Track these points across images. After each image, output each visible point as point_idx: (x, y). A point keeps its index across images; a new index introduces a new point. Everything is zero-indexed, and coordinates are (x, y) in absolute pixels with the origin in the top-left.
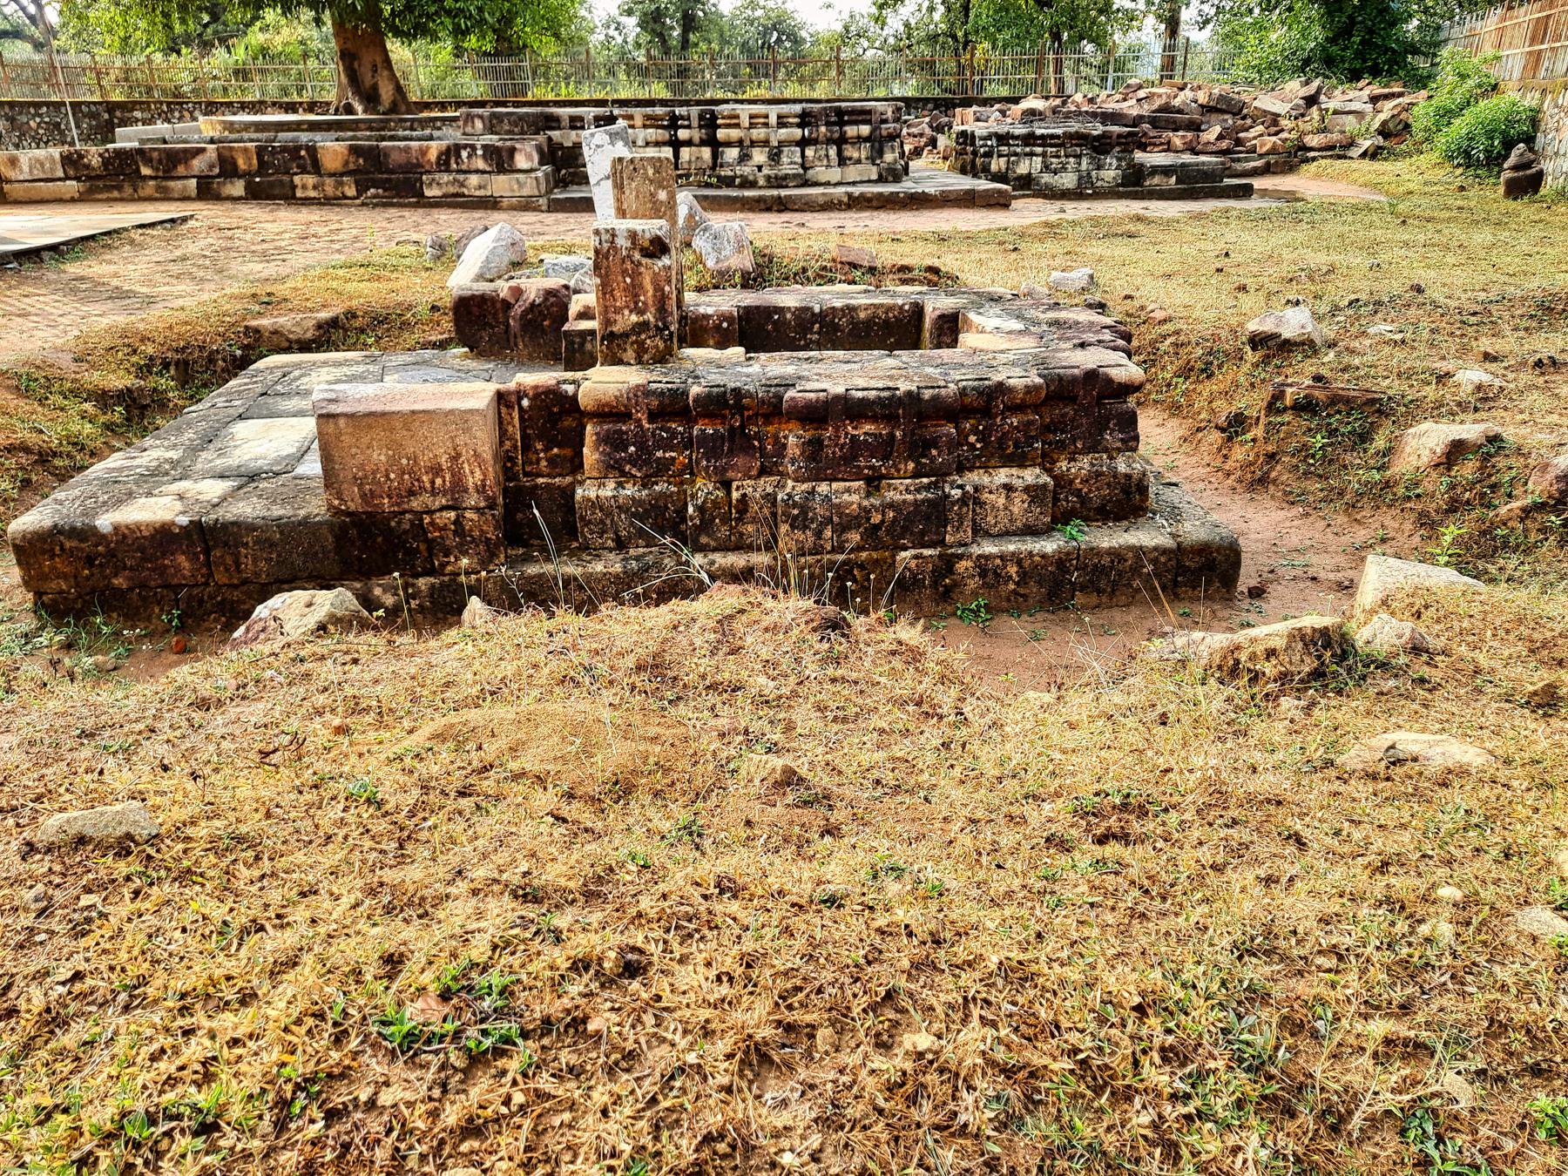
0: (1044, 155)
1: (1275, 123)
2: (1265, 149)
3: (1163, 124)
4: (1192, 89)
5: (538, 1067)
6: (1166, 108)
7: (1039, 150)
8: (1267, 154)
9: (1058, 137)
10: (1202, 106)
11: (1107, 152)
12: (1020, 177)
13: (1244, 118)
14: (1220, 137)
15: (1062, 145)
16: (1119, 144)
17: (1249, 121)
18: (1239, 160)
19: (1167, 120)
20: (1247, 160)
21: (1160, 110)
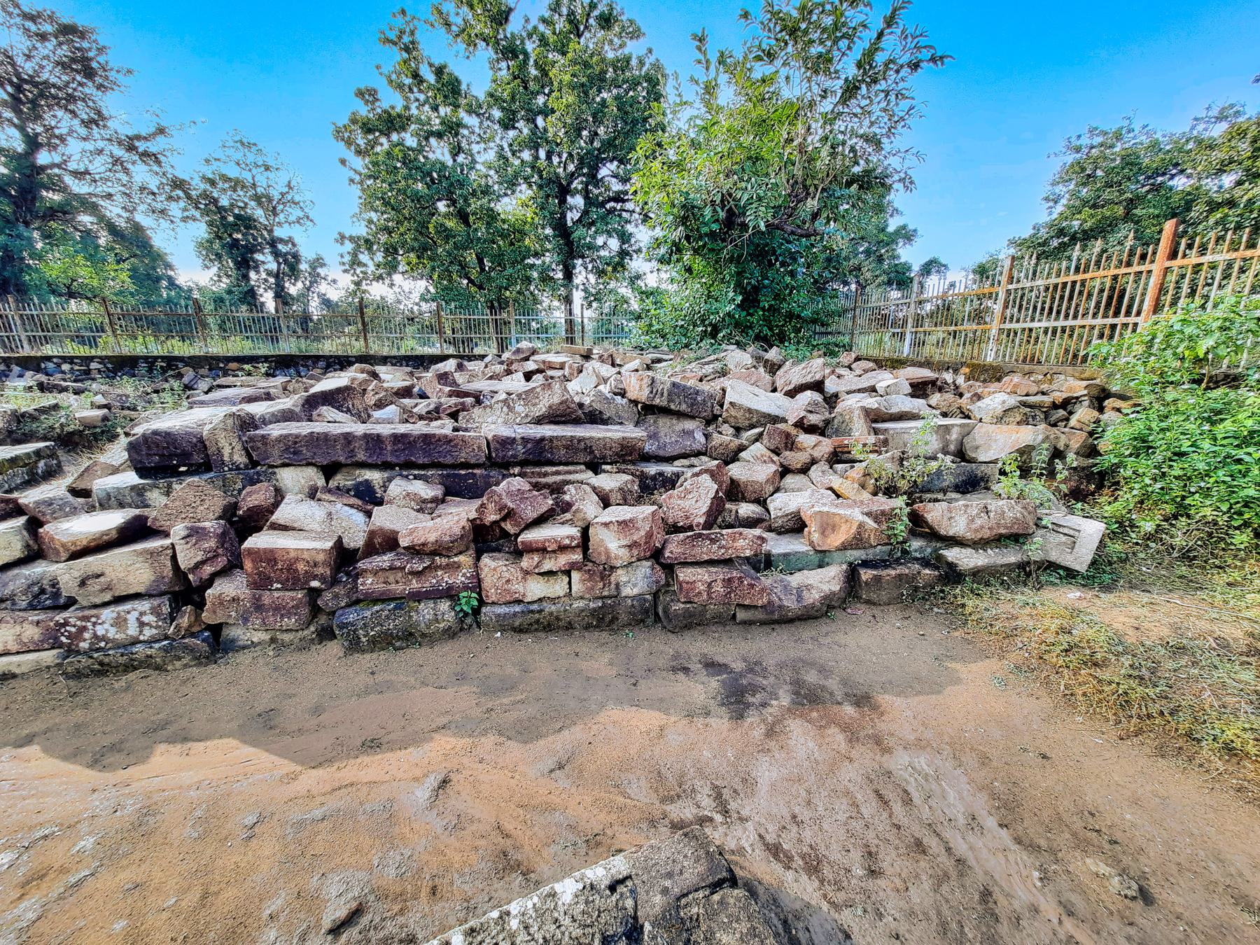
19: (572, 445)
21: (554, 417)
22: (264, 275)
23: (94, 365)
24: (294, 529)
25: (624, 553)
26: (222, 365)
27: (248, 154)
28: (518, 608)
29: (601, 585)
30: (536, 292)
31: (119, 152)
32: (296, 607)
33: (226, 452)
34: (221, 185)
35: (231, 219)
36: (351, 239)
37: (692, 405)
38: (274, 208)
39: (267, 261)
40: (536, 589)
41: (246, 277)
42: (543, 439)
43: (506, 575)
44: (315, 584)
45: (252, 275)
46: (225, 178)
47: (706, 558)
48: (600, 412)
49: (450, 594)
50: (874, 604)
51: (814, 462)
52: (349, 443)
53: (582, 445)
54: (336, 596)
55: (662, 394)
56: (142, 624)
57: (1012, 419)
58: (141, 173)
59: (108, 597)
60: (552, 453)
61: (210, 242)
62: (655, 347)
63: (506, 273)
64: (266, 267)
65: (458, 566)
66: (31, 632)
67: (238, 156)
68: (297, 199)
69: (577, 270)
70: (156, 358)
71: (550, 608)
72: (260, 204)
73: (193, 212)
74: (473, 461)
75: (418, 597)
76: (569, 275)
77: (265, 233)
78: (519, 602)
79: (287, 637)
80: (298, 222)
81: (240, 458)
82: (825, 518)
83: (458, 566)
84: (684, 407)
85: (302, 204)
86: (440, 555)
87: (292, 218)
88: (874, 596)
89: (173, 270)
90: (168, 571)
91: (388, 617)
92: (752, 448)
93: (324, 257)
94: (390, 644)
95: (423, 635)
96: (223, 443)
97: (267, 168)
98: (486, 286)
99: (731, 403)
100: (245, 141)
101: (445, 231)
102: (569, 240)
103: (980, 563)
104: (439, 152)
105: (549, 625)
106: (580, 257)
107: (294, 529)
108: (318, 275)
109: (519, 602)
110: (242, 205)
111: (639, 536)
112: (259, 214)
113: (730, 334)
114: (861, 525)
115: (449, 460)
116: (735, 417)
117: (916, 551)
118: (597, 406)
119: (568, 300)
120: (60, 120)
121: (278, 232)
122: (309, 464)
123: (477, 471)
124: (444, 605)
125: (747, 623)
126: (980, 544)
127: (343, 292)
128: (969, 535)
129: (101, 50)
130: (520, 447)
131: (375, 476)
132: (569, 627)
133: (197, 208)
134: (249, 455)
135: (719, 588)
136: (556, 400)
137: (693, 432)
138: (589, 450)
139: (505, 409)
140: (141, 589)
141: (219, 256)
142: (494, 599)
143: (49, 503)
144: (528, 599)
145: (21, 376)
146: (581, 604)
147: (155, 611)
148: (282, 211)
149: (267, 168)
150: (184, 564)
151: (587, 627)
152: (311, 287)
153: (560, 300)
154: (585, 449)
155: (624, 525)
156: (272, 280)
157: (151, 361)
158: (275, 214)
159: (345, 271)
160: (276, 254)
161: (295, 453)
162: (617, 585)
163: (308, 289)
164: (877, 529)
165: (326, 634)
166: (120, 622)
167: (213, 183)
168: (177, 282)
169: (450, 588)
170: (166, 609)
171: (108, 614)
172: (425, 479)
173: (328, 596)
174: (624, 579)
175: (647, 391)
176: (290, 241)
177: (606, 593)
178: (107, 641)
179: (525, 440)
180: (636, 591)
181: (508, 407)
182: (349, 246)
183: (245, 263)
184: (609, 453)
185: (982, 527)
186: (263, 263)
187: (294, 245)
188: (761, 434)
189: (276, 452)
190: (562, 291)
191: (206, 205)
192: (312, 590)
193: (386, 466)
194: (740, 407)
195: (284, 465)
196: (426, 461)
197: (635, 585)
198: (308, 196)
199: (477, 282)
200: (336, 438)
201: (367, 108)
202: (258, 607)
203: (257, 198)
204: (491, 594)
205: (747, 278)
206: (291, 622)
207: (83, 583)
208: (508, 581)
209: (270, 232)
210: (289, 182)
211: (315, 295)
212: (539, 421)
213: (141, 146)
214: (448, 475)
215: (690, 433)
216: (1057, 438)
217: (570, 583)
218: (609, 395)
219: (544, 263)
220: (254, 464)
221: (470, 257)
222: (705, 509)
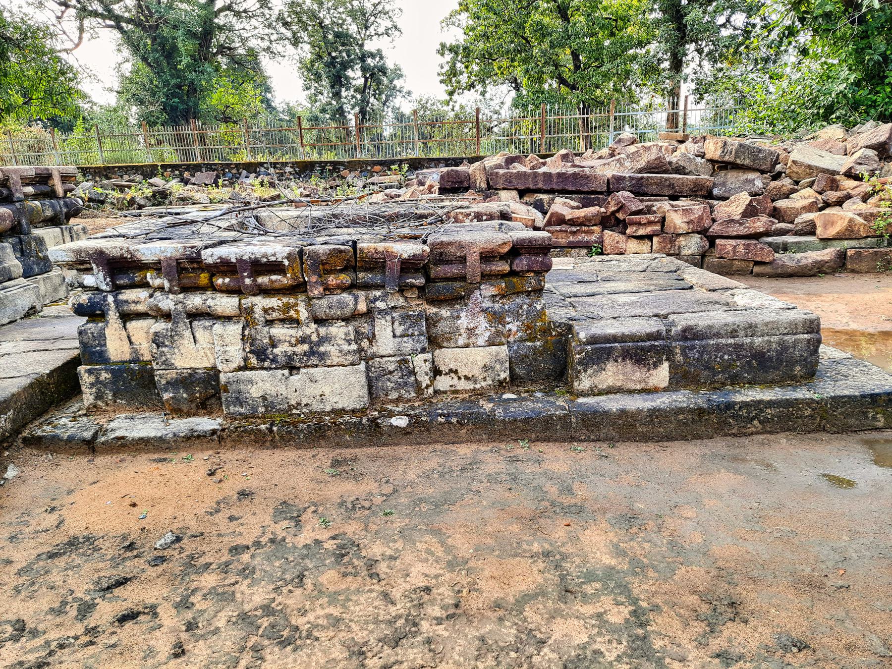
0: (245, 315)
1: (834, 185)
2: (832, 232)
3: (654, 189)
4: (695, 141)
5: (547, 554)
6: (657, 167)
7: (226, 304)
8: (839, 238)
9: (275, 267)
10: (712, 161)
11: (455, 299)
12: (187, 381)
13: (777, 177)
14: (750, 212)
15: (298, 288)
16: (487, 277)
17: (786, 183)
18: (785, 248)
19: (660, 183)
20: (800, 248)
21: (649, 169)
22: (352, 92)
23: (288, 169)
25: (684, 226)
26: (369, 168)
29: (669, 246)
30: (634, 87)
33: (478, 181)
37: (754, 160)
38: (367, 21)
39: (356, 76)
47: (735, 233)
48: (684, 168)
50: (858, 272)
51: (849, 197)
55: (731, 153)
60: (647, 188)
62: (762, 133)
63: (604, 69)
68: (387, 8)
69: (689, 57)
70: (326, 163)
72: (355, 19)
74: (599, 190)
76: (677, 65)
80: (387, 34)
81: (484, 185)
82: (827, 217)
83: (592, 232)
84: (747, 162)
85: (390, 13)
86: (585, 225)
87: (381, 30)
88: (856, 267)
89: (270, 92)
92: (802, 191)
93: (402, 67)
96: (478, 177)
98: (580, 85)
99: (793, 161)
101: (541, 29)
102: (681, 23)
106: (692, 41)
108: (395, 87)
110: (340, 22)
112: (353, 29)
113: (846, 115)
114: (851, 221)
115: (585, 189)
116: (797, 173)
118: (681, 163)
119: (674, 93)
121: (370, 46)
123: (601, 196)
125: (760, 275)
127: (416, 104)
131: (545, 197)
134: (488, 183)
135: (741, 249)
136: (653, 157)
137: (754, 180)
138: (672, 186)
139: (618, 165)
141: (318, 77)
142: (609, 251)
145: (247, 177)
153: (663, 95)
155: (686, 211)
156: (359, 96)
157: (323, 164)
158: (367, 28)
159: (442, 82)
162: (679, 247)
164: (865, 225)
168: (273, 104)
169: (588, 242)
172: (572, 199)
174: (684, 243)
175: (719, 151)
176: (379, 54)
180: (690, 252)
181: (620, 163)
182: (448, 57)
183: (338, 81)
186: (354, 79)
187: (381, 58)
188: (813, 182)
190: (668, 84)
193: (551, 191)
194: (802, 164)
195: (504, 189)
196: (573, 189)
197: (690, 248)
198: (395, 5)
199: (570, 81)
205: (869, 54)
208: (618, 242)
209: (361, 46)
211: (390, 109)
214: (584, 198)
215: (752, 181)
217: (651, 246)
218: (692, 157)
219: (648, 52)
220: (489, 187)
221: (565, 56)
222: (741, 211)
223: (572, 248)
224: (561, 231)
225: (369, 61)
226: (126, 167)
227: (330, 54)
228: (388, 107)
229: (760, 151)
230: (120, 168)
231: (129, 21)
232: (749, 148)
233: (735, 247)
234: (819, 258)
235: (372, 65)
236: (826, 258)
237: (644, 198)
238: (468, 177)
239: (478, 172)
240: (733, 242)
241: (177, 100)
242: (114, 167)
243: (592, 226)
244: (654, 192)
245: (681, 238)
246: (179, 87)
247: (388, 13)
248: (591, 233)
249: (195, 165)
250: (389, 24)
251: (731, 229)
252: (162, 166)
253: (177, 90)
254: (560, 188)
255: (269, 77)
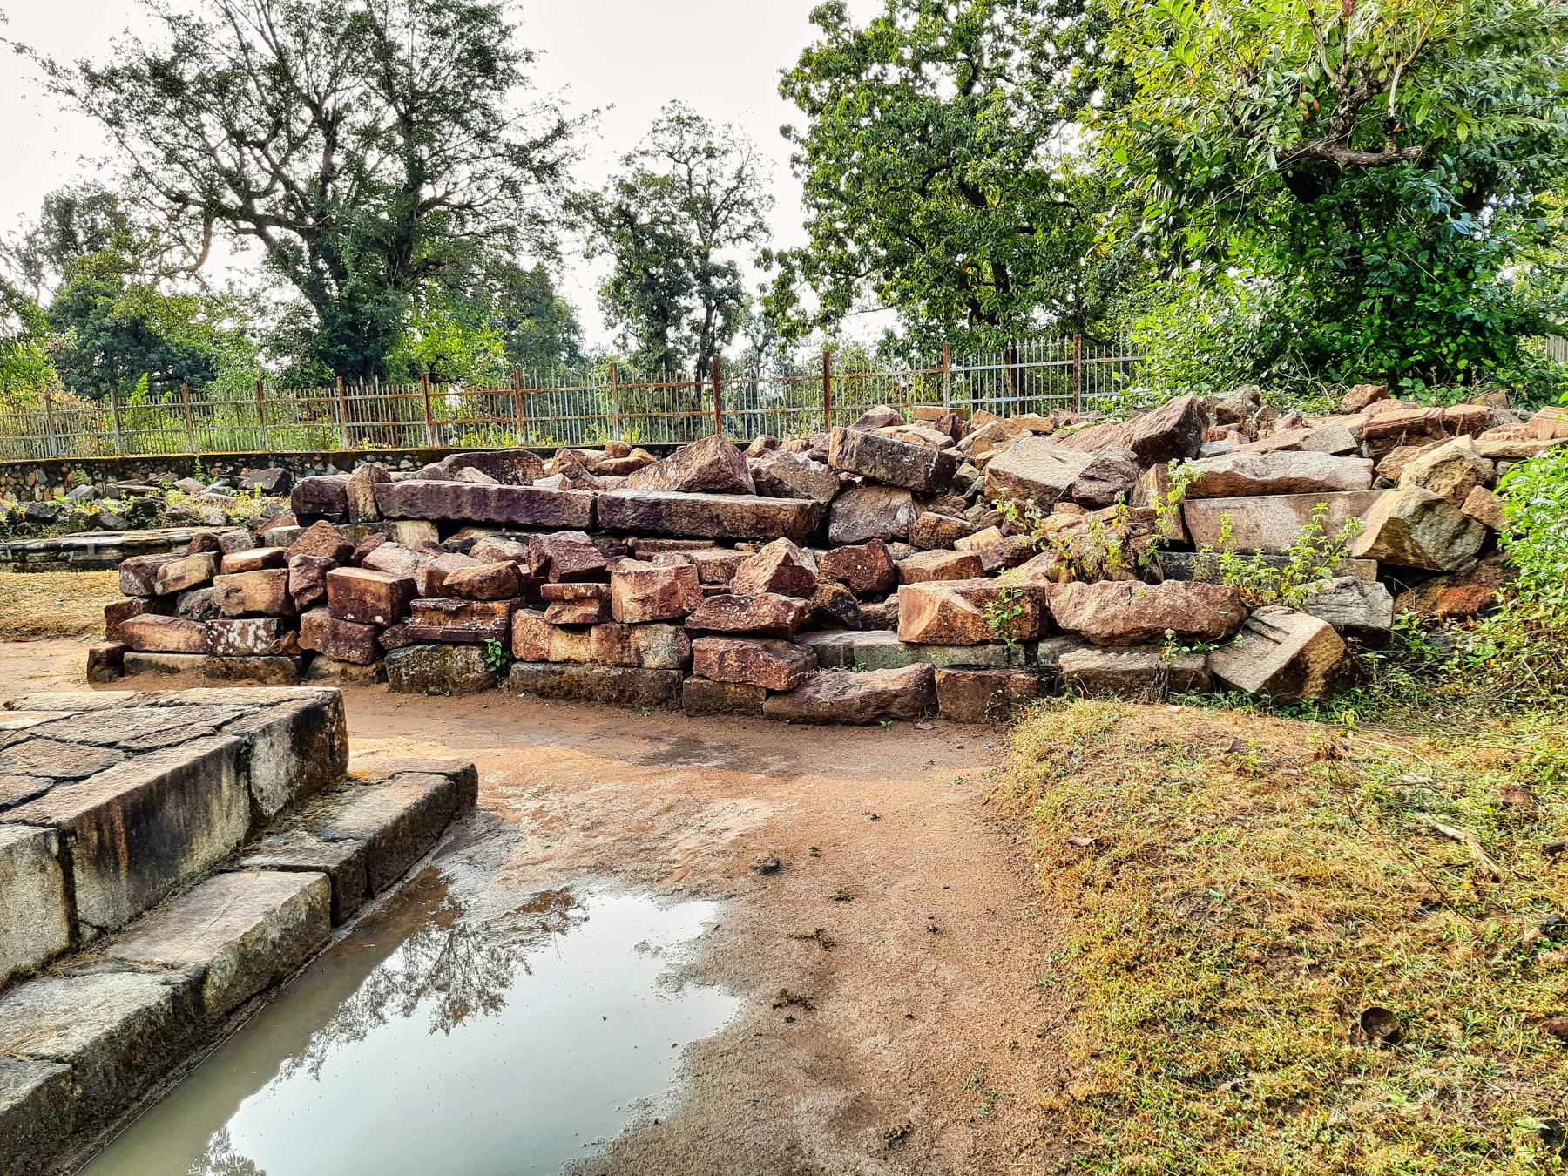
3: (683, 524)
22: (686, 331)
24: (379, 569)
27: (686, 136)
28: (541, 667)
31: (509, 170)
32: (361, 640)
33: (361, 502)
34: (642, 193)
35: (650, 245)
36: (782, 259)
37: (894, 470)
38: (715, 216)
39: (694, 306)
40: (561, 647)
41: (661, 336)
42: (657, 503)
43: (535, 628)
44: (379, 619)
45: (671, 333)
46: (649, 180)
47: (731, 626)
48: (781, 482)
49: (476, 640)
50: (957, 721)
52: (458, 497)
53: (706, 513)
54: (395, 634)
56: (257, 638)
57: (1445, 481)
58: (534, 195)
59: (240, 611)
61: (618, 285)
64: (692, 316)
65: (492, 614)
66: (196, 638)
67: (671, 141)
68: (749, 196)
71: (571, 670)
72: (694, 213)
73: (601, 240)
75: (456, 640)
77: (696, 261)
78: (545, 661)
79: (353, 671)
80: (746, 236)
83: (492, 614)
84: (881, 472)
85: (756, 204)
86: (477, 599)
87: (739, 230)
89: (576, 332)
90: (281, 595)
91: (426, 658)
94: (425, 687)
95: (455, 685)
96: (359, 494)
97: (711, 154)
99: (991, 471)
100: (684, 115)
103: (1091, 665)
104: (943, 84)
105: (570, 692)
107: (379, 569)
109: (545, 661)
111: (653, 589)
112: (692, 231)
114: (945, 607)
117: (1046, 657)
120: (456, 139)
122: (423, 519)
124: (475, 654)
126: (1109, 643)
128: (1094, 629)
129: (504, 33)
130: (629, 511)
132: (590, 698)
133: (607, 233)
135: (732, 661)
138: (714, 519)
140: (261, 607)
143: (233, 540)
144: (552, 659)
146: (602, 670)
147: (267, 628)
148: (725, 221)
149: (711, 154)
150: (293, 589)
151: (608, 701)
152: (765, 345)
154: (711, 518)
156: (697, 338)
158: (715, 227)
160: (708, 294)
161: (411, 506)
162: (637, 650)
163: (760, 351)
164: (975, 617)
165: (381, 676)
166: (243, 633)
167: (630, 190)
169: (478, 634)
170: (274, 627)
171: (237, 624)
173: (388, 633)
174: (643, 643)
177: (626, 660)
178: (235, 649)
179: (636, 503)
183: (662, 315)
184: (742, 525)
185: (1114, 617)
187: (735, 275)
189: (396, 504)
191: (619, 227)
192: (377, 624)
195: (403, 518)
197: (656, 653)
200: (446, 492)
201: (827, 37)
202: (335, 636)
203: (690, 205)
204: (520, 650)
206: (356, 655)
207: (227, 596)
210: (740, 171)
212: (688, 488)
213: (536, 157)
216: (1494, 510)
223: (456, 644)
224: (436, 609)
225: (714, 280)
226: (154, 459)
227: (646, 271)
228: (768, 355)
229: (905, 451)
230: (144, 461)
231: (279, 222)
232: (882, 445)
233: (722, 655)
234: (880, 686)
235: (718, 287)
236: (894, 687)
237: (665, 542)
238: (343, 494)
239: (359, 486)
240: (722, 644)
241: (344, 347)
242: (136, 460)
243: (492, 599)
244: (686, 531)
245: (638, 633)
246: (353, 326)
247: (750, 203)
248: (488, 614)
249: (258, 456)
250: (749, 220)
251: (724, 617)
252: (203, 459)
253: (347, 332)
254: (503, 518)
255: (572, 309)
